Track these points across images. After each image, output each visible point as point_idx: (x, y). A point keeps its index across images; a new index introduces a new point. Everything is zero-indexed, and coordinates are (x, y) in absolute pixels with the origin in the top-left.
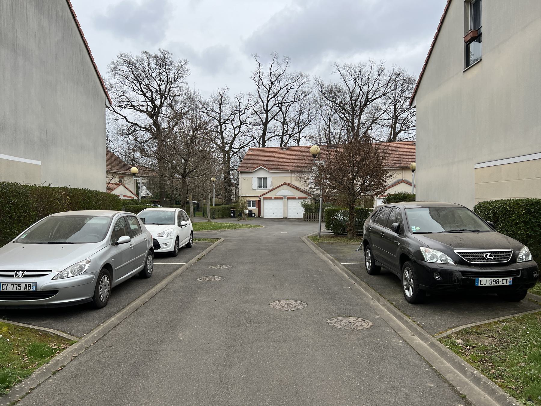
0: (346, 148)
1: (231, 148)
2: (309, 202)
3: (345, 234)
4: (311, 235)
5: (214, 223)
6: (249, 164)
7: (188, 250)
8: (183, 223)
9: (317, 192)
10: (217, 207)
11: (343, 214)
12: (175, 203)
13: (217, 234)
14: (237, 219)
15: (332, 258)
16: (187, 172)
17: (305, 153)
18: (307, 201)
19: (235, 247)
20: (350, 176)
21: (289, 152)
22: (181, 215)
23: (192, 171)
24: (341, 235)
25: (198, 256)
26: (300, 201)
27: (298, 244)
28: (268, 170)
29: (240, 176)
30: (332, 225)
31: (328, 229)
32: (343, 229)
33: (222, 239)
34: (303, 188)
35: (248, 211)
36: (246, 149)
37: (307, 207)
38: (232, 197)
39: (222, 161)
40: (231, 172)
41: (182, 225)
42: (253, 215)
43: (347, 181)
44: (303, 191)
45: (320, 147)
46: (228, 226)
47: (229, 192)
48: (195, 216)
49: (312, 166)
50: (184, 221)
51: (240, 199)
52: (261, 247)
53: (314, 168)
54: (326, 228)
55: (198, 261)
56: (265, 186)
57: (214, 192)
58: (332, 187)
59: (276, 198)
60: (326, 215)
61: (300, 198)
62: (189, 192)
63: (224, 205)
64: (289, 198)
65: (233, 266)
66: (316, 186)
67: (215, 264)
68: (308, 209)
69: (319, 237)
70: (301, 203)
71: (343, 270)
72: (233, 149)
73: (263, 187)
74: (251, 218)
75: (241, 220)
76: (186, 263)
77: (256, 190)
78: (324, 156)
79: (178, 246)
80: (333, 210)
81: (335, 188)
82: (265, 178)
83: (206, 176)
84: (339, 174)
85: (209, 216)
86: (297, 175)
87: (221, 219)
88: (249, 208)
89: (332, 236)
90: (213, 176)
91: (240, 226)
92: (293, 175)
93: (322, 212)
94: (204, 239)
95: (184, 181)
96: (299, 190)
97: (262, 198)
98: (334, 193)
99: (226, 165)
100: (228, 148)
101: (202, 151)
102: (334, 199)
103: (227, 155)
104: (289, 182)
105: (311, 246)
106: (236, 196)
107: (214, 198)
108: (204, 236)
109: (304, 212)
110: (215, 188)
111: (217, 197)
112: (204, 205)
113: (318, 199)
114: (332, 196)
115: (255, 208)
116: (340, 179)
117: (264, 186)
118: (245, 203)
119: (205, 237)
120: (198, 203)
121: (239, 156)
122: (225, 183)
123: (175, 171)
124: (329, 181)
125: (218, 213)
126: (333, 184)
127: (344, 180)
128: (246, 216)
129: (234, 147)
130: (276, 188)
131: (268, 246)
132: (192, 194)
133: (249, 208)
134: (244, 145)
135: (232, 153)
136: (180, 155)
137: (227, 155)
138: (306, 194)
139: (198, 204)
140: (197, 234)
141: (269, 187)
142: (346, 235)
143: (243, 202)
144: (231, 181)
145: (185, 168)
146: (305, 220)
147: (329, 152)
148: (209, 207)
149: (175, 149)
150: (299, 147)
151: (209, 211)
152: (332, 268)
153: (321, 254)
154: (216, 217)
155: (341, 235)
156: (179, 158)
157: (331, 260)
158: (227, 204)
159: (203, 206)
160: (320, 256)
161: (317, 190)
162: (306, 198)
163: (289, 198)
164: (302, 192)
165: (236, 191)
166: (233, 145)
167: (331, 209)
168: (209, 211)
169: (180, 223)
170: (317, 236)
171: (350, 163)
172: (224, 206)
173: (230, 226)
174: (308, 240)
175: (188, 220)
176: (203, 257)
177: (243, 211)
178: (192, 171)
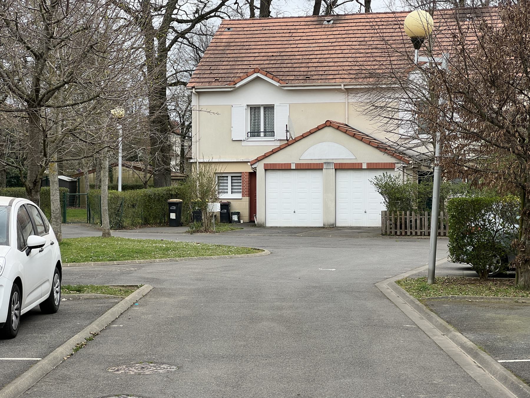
0: (511, 18)
1: (168, 19)
2: (401, 177)
3: (508, 272)
4: (406, 275)
5: (122, 240)
6: (223, 68)
7: (48, 319)
8: (32, 240)
9: (422, 150)
10: (129, 193)
11: (503, 215)
12: (5, 181)
13: (130, 272)
14: (187, 229)
15: (470, 344)
16: (42, 91)
17: (388, 32)
18: (392, 174)
19: (186, 312)
20: (524, 100)
21: (339, 28)
22: (25, 217)
23: (58, 88)
24: (493, 276)
25: (78, 338)
26: (372, 176)
27: (369, 304)
28: (277, 84)
29: (194, 101)
30: (469, 248)
31: (458, 260)
32: (502, 257)
33: (146, 288)
34: (381, 136)
35: (218, 205)
36: (214, 23)
37: (395, 193)
38: (173, 163)
39: (145, 58)
40: (168, 92)
41: (31, 248)
42: (235, 218)
43: (514, 116)
44: (381, 147)
45: (432, 15)
46: (161, 249)
47: (162, 151)
48: (64, 222)
49: (408, 73)
50: (36, 233)
51: (195, 172)
52: (260, 312)
53: (416, 77)
54: (452, 254)
55: (76, 350)
56: (270, 132)
57: (120, 151)
58: (469, 136)
59: (302, 168)
60: (453, 216)
61: (372, 167)
62: (48, 151)
63: (150, 186)
64: (340, 167)
65: (179, 368)
66: (422, 131)
67: (128, 362)
68: (398, 199)
69: (430, 281)
70: (375, 181)
71: (504, 380)
72: (175, 24)
73: (262, 134)
74: (227, 226)
75: (198, 231)
76: (43, 357)
77: (243, 144)
78: (446, 42)
79: (19, 309)
80: (473, 201)
81: (477, 137)
82: (269, 109)
83: (98, 102)
84: (488, 94)
85: (106, 219)
86: (364, 98)
87: (141, 230)
88: (222, 196)
89: (471, 280)
90: (117, 103)
91: (196, 249)
92: (353, 99)
93: (440, 207)
94: (92, 287)
95: (34, 118)
96: (369, 143)
97: (260, 168)
98: (474, 151)
99: (157, 70)
100: (162, 19)
101: (86, 29)
102: (476, 171)
103: (156, 43)
104: (339, 119)
105: (408, 309)
106: (182, 163)
107: (120, 168)
108: (93, 280)
109: (385, 209)
110: (124, 137)
111: (129, 163)
112: (92, 187)
113: (424, 169)
114: (469, 160)
115: (239, 196)
116: (492, 109)
117: (265, 132)
118: (210, 180)
119: (96, 282)
120: (72, 182)
121: (191, 44)
122: (153, 122)
123: (10, 88)
124: (461, 117)
125: (131, 210)
126: (471, 125)
127: (506, 111)
128: (213, 221)
129: (179, 18)
130: (303, 137)
131: (280, 308)
132: (56, 156)
133: (222, 196)
134: (207, 10)
135: (171, 36)
136: (21, 40)
137: (156, 43)
138: (392, 155)
139: (73, 186)
140: (71, 274)
141: (280, 133)
142: (513, 276)
143: (205, 181)
144: (168, 117)
145: (38, 80)
146: (388, 232)
147: (460, 29)
148: (105, 193)
149: (8, 25)
150: (370, 16)
151: (105, 206)
152: (471, 373)
153: (439, 333)
154: (127, 222)
155: (493, 276)
156: (18, 49)
157: (470, 351)
158: (156, 184)
159: (88, 191)
160: (434, 338)
161: (424, 143)
162: (390, 167)
163: (340, 167)
164: (377, 148)
165: (182, 146)
166: (175, 11)
167: (466, 201)
168: (105, 206)
169: (25, 242)
170: (424, 280)
171: (523, 63)
172: (149, 191)
173: (167, 249)
174: (399, 292)
175: (46, 231)
176: (90, 339)
177: (203, 205)
178: (58, 88)
